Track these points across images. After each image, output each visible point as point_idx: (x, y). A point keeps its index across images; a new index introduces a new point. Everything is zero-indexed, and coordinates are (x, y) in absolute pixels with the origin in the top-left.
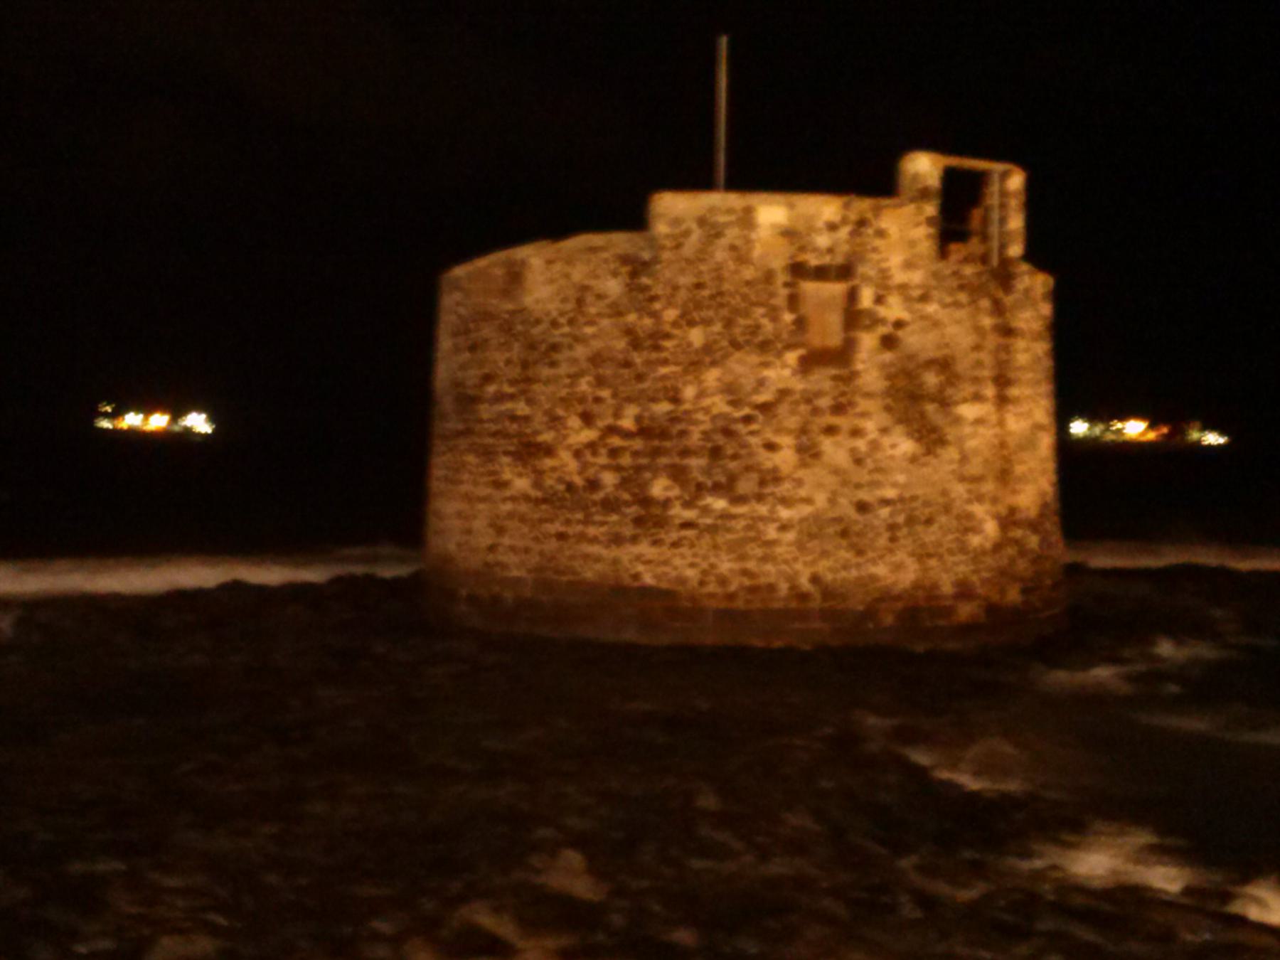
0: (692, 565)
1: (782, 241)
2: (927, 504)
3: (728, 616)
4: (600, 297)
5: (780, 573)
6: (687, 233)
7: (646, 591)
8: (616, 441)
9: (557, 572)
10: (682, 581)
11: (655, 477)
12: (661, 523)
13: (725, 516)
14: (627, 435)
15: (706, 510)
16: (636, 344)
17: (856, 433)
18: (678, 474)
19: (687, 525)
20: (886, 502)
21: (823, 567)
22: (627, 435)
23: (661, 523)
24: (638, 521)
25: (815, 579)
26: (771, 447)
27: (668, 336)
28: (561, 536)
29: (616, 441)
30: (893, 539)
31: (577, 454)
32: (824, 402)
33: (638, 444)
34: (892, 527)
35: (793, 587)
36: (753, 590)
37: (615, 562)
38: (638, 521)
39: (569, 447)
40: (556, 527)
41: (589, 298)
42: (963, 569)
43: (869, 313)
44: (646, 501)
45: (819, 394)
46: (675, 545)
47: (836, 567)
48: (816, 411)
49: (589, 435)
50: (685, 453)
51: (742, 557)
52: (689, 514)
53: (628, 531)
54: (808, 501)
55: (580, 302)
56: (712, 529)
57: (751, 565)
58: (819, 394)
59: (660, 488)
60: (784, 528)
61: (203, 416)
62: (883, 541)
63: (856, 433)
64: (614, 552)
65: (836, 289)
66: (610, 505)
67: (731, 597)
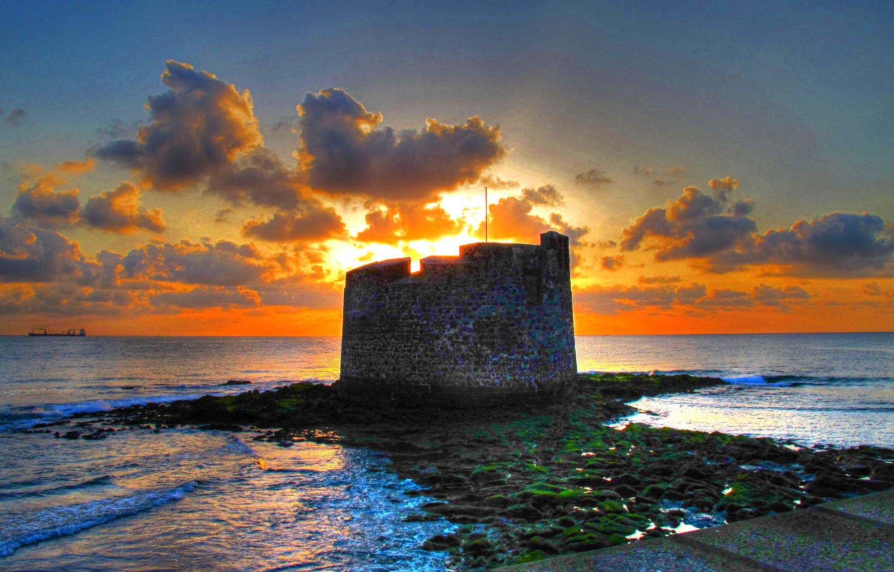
0: (498, 378)
5: (526, 379)
6: (490, 257)
8: (466, 333)
10: (494, 385)
14: (470, 330)
15: (502, 358)
22: (470, 330)
24: (476, 363)
25: (536, 381)
27: (484, 294)
29: (466, 333)
31: (450, 338)
32: (535, 318)
35: (530, 384)
37: (469, 378)
39: (445, 336)
41: (453, 280)
47: (878, 442)
49: (452, 331)
50: (494, 337)
54: (533, 353)
55: (449, 281)
56: (503, 365)
57: (517, 377)
60: (526, 363)
61: (365, 131)
64: (468, 374)
65: (534, 278)
67: (512, 389)
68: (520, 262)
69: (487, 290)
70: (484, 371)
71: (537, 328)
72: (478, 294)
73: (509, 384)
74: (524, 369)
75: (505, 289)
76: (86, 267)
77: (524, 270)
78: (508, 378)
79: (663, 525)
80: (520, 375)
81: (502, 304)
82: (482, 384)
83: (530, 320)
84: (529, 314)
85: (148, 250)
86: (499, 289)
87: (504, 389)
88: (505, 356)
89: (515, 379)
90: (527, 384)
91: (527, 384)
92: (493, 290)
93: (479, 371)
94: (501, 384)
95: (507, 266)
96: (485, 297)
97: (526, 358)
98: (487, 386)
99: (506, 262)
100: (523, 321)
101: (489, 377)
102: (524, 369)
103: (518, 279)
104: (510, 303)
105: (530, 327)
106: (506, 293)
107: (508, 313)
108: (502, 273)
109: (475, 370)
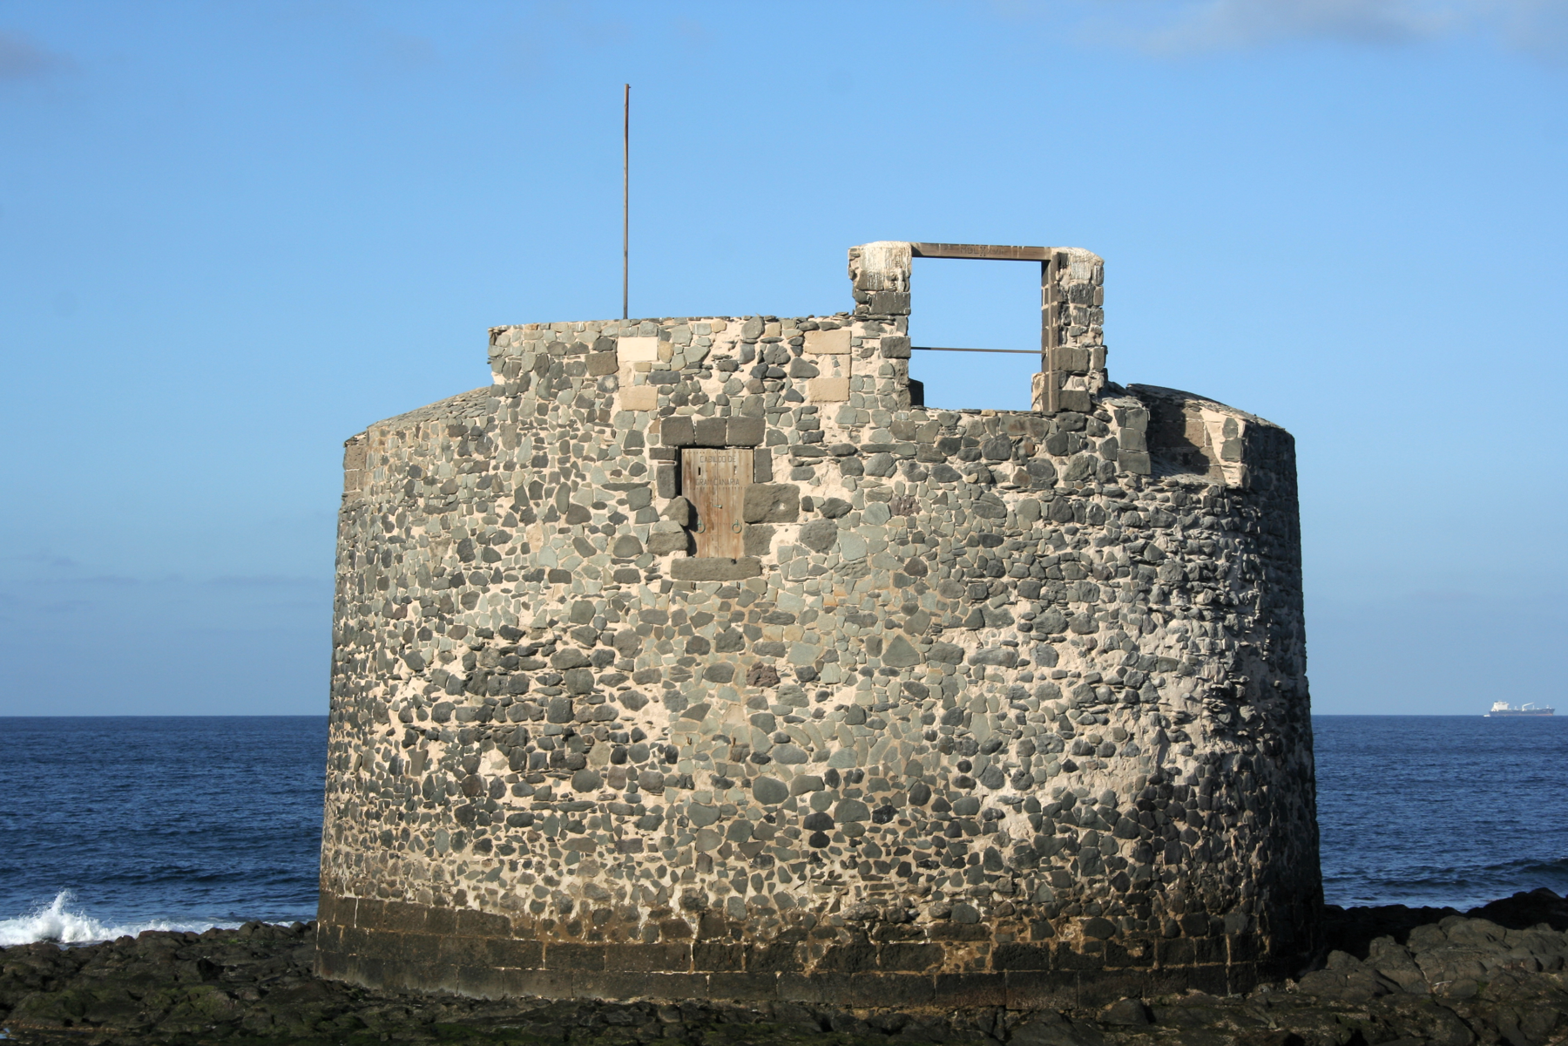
0: (527, 880)
1: (652, 390)
2: (878, 785)
3: (573, 959)
4: (431, 482)
6: (526, 382)
7: (477, 920)
9: (382, 893)
11: (485, 747)
12: (490, 814)
13: (569, 805)
15: (545, 798)
16: (465, 553)
17: (764, 677)
18: (513, 745)
19: (522, 820)
20: (804, 785)
21: (704, 881)
23: (490, 814)
24: (465, 816)
25: (690, 903)
26: (635, 703)
27: (504, 538)
28: (387, 839)
29: (443, 697)
30: (819, 841)
32: (709, 632)
33: (471, 702)
34: (819, 823)
35: (660, 913)
36: (604, 916)
37: (438, 874)
38: (465, 816)
40: (379, 827)
42: (954, 886)
43: (787, 492)
44: (471, 785)
45: (703, 619)
46: (506, 849)
48: (698, 646)
49: (417, 687)
50: (524, 712)
51: (590, 869)
52: (525, 802)
53: (452, 828)
54: (686, 782)
57: (600, 880)
58: (703, 619)
59: (492, 765)
62: (804, 842)
63: (764, 677)
65: (736, 461)
66: (434, 793)
67: (574, 928)
68: (651, 396)
69: (509, 521)
70: (485, 847)
71: (717, 675)
72: (482, 539)
73: (568, 909)
74: (637, 845)
75: (578, 515)
76: (499, 748)
77: (485, 447)
78: (567, 880)
79: (731, 427)
80: (615, 871)
81: (560, 576)
82: (474, 905)
83: (680, 642)
84: (679, 616)
85: (986, 855)
86: (551, 516)
87: (549, 924)
88: (565, 787)
89: (590, 889)
90: (644, 912)
91: (644, 912)
92: (528, 518)
93: (469, 847)
94: (537, 907)
95: (591, 418)
96: (501, 549)
97: (649, 801)
98: (488, 910)
99: (581, 401)
100: (648, 644)
101: (494, 876)
102: (637, 845)
103: (638, 469)
104: (592, 573)
105: (680, 674)
106: (576, 529)
107: (582, 613)
108: (565, 448)
109: (458, 844)
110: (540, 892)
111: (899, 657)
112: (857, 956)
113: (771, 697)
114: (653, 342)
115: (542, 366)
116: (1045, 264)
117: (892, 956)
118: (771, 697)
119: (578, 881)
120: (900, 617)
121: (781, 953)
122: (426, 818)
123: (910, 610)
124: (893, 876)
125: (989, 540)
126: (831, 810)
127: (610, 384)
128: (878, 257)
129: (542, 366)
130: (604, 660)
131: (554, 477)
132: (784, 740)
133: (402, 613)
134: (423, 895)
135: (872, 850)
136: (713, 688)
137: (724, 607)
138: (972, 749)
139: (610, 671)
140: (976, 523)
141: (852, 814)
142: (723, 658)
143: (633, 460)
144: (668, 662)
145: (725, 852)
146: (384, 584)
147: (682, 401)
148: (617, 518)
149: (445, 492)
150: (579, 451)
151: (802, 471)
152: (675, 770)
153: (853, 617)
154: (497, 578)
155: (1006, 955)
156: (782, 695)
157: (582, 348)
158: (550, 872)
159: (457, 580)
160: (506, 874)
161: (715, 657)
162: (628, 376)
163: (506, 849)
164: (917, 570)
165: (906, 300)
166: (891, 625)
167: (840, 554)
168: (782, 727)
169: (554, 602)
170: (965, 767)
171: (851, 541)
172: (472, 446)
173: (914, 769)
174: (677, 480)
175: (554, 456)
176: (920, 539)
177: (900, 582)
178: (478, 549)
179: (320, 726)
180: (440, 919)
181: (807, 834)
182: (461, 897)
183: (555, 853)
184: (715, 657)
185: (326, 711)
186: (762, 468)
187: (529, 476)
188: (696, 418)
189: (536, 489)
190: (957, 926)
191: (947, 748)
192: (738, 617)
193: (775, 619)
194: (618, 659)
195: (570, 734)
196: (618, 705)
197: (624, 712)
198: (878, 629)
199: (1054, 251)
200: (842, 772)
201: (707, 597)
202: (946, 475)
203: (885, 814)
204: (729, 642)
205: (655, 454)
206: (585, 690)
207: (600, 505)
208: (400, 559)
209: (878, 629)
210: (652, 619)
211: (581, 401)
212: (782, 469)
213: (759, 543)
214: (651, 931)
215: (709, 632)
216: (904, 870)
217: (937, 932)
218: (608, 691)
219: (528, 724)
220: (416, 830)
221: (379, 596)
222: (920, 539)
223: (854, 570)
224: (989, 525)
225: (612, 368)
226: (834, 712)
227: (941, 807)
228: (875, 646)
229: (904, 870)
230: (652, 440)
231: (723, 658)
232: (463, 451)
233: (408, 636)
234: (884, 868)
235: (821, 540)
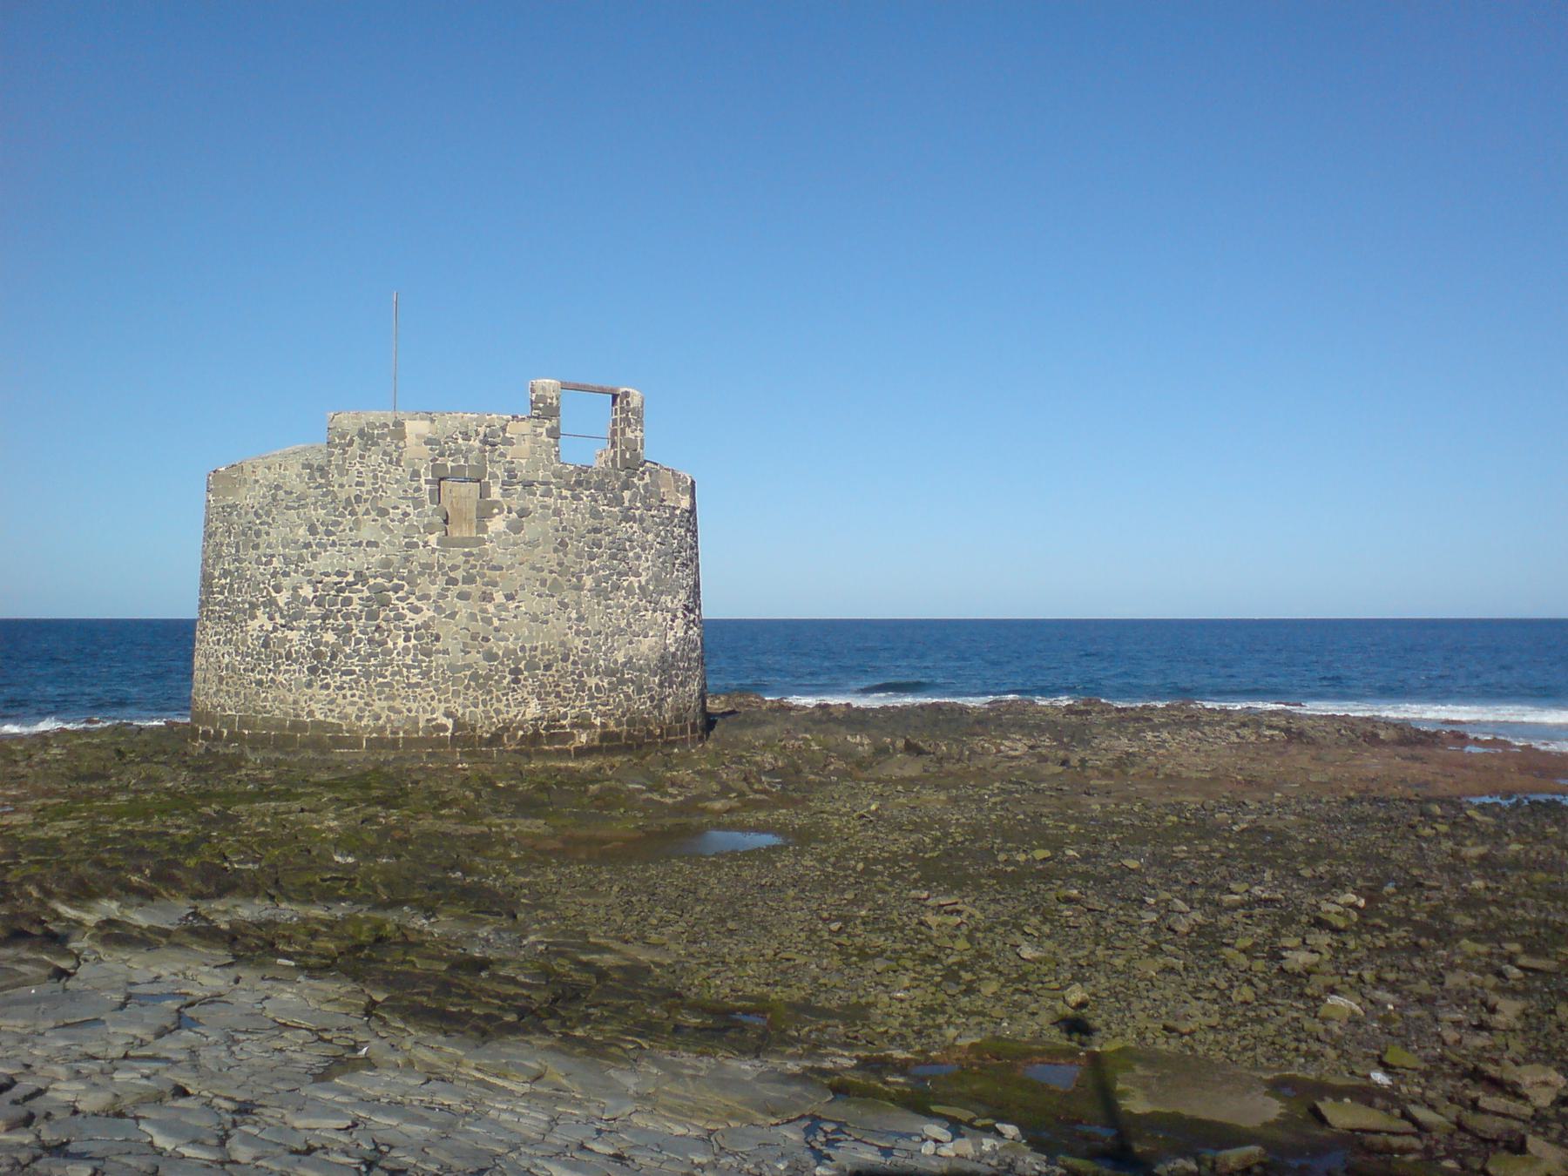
0: (353, 704)
9: (256, 711)
16: (312, 530)
21: (456, 706)
28: (260, 683)
32: (459, 574)
34: (516, 672)
48: (452, 581)
58: (454, 568)
67: (383, 728)
71: (463, 596)
73: (378, 718)
75: (383, 512)
95: (391, 462)
98: (330, 720)
103: (418, 489)
105: (442, 596)
108: (375, 477)
110: (360, 709)
111: (555, 587)
112: (535, 738)
113: (491, 608)
114: (427, 423)
115: (361, 434)
116: (615, 397)
117: (552, 738)
118: (491, 608)
119: (385, 704)
120: (556, 568)
121: (496, 739)
122: (286, 671)
123: (560, 564)
124: (552, 698)
125: (596, 530)
126: (522, 666)
127: (401, 444)
128: (548, 384)
129: (361, 434)
130: (396, 589)
131: (368, 492)
132: (497, 630)
133: (269, 563)
134: (286, 713)
135: (542, 685)
136: (460, 603)
137: (467, 562)
138: (587, 633)
139: (401, 594)
140: (590, 522)
141: (532, 666)
142: (466, 588)
143: (415, 484)
144: (434, 590)
145: (467, 687)
146: (256, 547)
147: (442, 454)
148: (406, 514)
149: (299, 498)
150: (383, 479)
151: (506, 493)
152: (439, 645)
153: (533, 568)
154: (334, 544)
155: (606, 736)
156: (497, 607)
157: (386, 425)
158: (368, 699)
159: (307, 545)
160: (340, 700)
161: (461, 587)
162: (411, 439)
163: (341, 688)
164: (563, 544)
165: (558, 408)
166: (551, 572)
167: (526, 535)
168: (496, 622)
169: (377, 556)
170: (586, 643)
171: (531, 529)
172: (317, 474)
173: (563, 644)
174: (436, 496)
175: (369, 482)
176: (564, 529)
177: (556, 550)
178: (321, 529)
179: (193, 623)
180: (297, 726)
181: (509, 678)
182: (311, 714)
183: (370, 689)
184: (461, 587)
185: (197, 616)
186: (484, 492)
187: (355, 491)
188: (449, 464)
189: (358, 498)
190: (583, 723)
191: (578, 633)
192: (474, 567)
193: (494, 568)
194: (406, 587)
195: (378, 627)
196: (406, 612)
197: (410, 615)
198: (545, 574)
199: (623, 390)
200: (528, 646)
201: (457, 556)
202: (576, 498)
203: (548, 667)
204: (469, 580)
205: (427, 482)
206: (385, 603)
207: (396, 508)
208: (268, 534)
209: (545, 574)
210: (426, 567)
211: (385, 453)
212: (496, 492)
213: (483, 529)
214: (426, 729)
215: (459, 574)
216: (558, 695)
217: (573, 726)
218: (400, 604)
219: (353, 622)
220: (280, 678)
221: (253, 554)
222: (564, 529)
223: (533, 544)
224: (596, 523)
225: (403, 437)
226: (524, 618)
227: (574, 663)
228: (543, 582)
229: (558, 695)
230: (426, 475)
231: (466, 588)
232: (311, 477)
233: (274, 575)
234: (548, 694)
235: (515, 528)
